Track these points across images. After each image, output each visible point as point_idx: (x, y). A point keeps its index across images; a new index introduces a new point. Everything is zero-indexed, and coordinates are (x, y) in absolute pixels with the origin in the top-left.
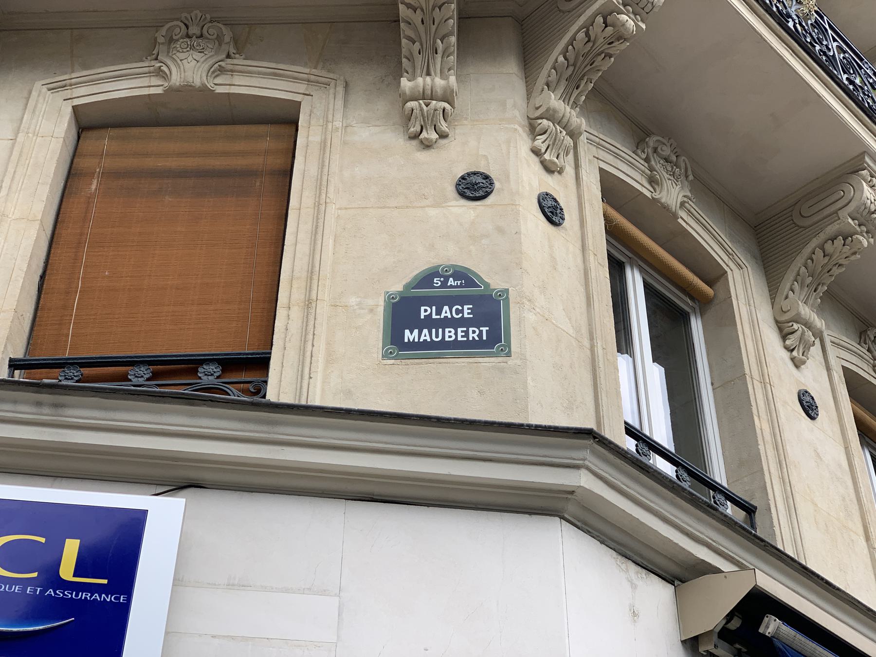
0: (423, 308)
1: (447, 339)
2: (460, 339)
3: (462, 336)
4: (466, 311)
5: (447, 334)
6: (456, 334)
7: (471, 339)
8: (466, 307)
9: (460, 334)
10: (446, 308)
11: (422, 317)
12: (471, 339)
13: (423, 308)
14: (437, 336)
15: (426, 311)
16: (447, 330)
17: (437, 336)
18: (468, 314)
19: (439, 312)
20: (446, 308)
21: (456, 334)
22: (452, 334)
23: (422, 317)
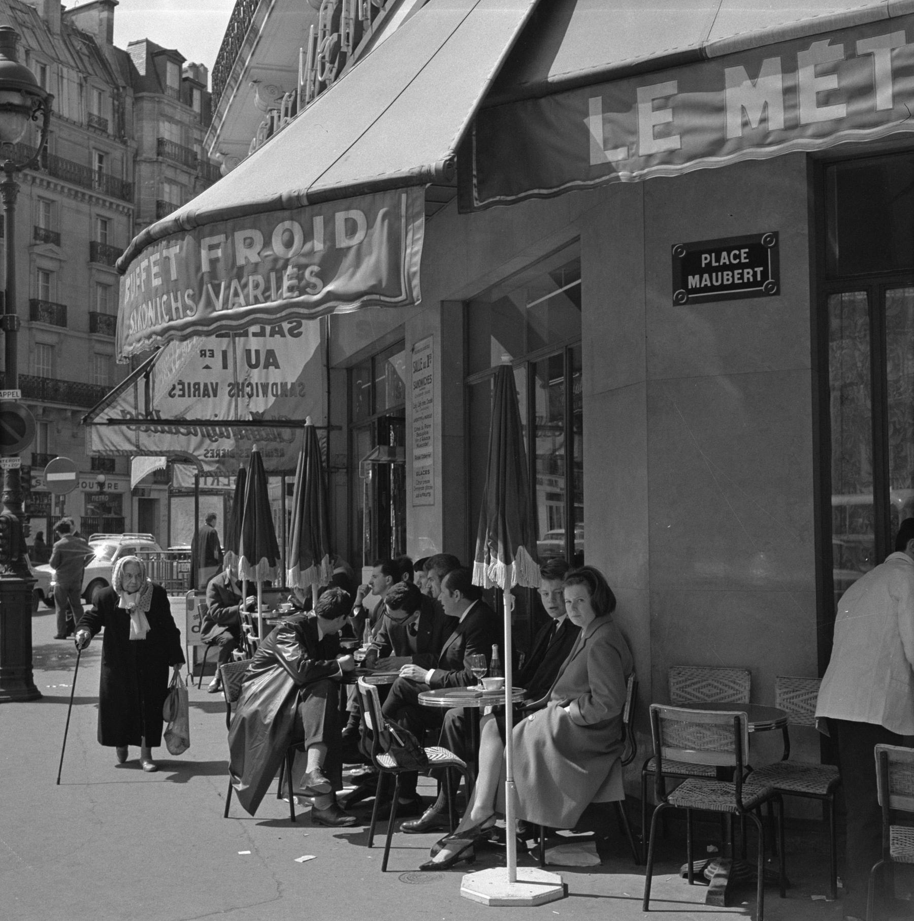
0: (703, 256)
1: (725, 282)
2: (736, 281)
3: (739, 279)
4: (743, 256)
5: (725, 277)
6: (733, 277)
7: (746, 280)
8: (743, 251)
9: (737, 276)
10: (724, 254)
11: (703, 265)
12: (746, 280)
13: (703, 256)
14: (717, 281)
15: (706, 259)
16: (725, 273)
17: (717, 281)
18: (745, 258)
19: (718, 260)
20: (724, 254)
21: (733, 277)
22: (730, 277)
23: (703, 265)
